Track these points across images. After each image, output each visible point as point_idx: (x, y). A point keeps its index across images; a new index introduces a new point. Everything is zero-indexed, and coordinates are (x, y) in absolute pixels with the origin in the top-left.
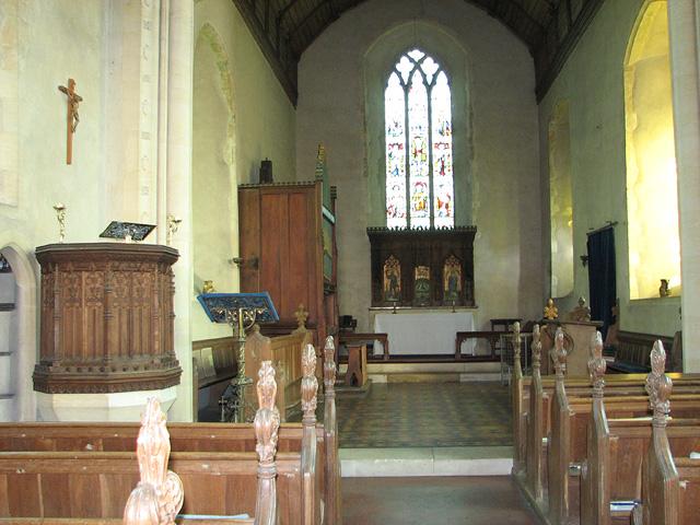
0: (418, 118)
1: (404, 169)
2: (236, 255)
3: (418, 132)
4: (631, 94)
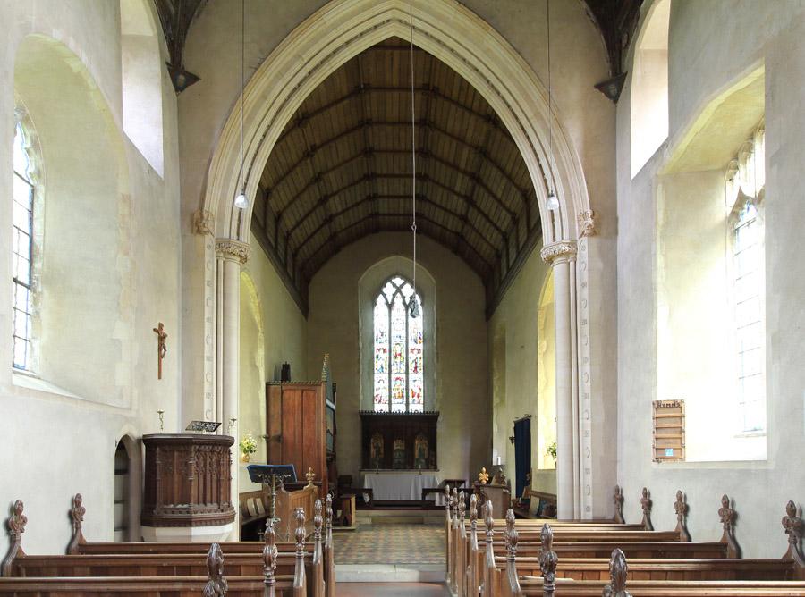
0: (398, 330)
1: (387, 367)
2: (264, 433)
3: (398, 340)
4: (542, 327)
